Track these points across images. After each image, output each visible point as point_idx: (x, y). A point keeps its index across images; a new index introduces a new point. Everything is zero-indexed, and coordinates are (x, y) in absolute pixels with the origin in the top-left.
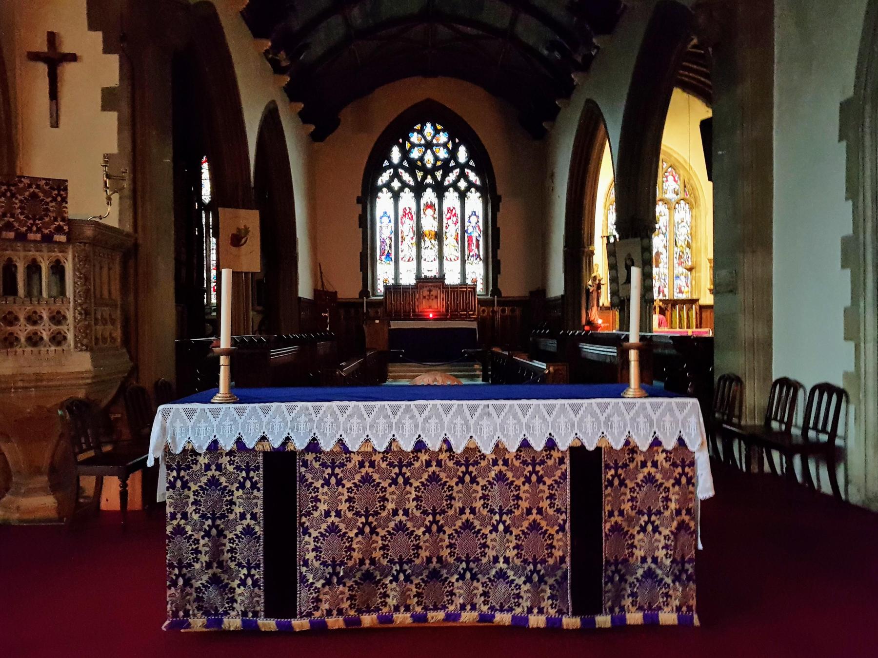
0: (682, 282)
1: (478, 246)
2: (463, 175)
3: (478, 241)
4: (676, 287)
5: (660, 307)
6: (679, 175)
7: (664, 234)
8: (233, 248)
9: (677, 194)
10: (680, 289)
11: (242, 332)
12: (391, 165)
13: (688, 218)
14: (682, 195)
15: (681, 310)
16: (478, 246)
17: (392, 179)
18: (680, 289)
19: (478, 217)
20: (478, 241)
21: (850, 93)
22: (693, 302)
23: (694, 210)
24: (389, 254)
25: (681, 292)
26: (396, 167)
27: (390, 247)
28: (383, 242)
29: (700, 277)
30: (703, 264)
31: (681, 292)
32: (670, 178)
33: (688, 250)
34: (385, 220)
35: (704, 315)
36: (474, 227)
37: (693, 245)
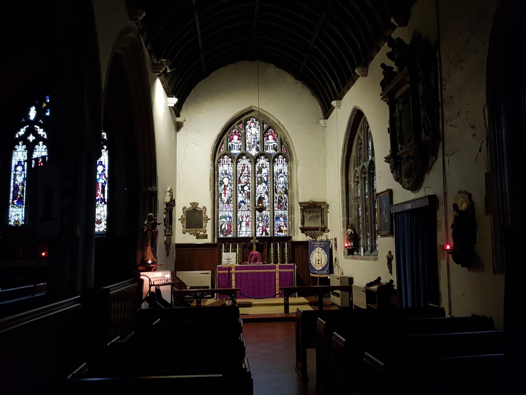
0: (281, 222)
1: (103, 192)
2: (31, 131)
3: (103, 187)
4: (276, 226)
5: (257, 244)
6: (277, 134)
7: (266, 182)
8: (431, 193)
9: (276, 150)
10: (280, 228)
11: (274, 271)
12: (28, 122)
13: (285, 170)
14: (279, 151)
15: (275, 247)
16: (103, 192)
17: (27, 134)
18: (280, 228)
19: (104, 166)
20: (103, 187)
21: (382, 77)
22: (287, 239)
23: (289, 163)
24: (21, 198)
25: (281, 231)
26: (32, 123)
27: (23, 192)
28: (16, 187)
29: (294, 217)
30: (296, 207)
31: (281, 231)
32: (270, 137)
33: (285, 195)
34: (19, 168)
35: (296, 250)
36: (100, 175)
37: (289, 191)
